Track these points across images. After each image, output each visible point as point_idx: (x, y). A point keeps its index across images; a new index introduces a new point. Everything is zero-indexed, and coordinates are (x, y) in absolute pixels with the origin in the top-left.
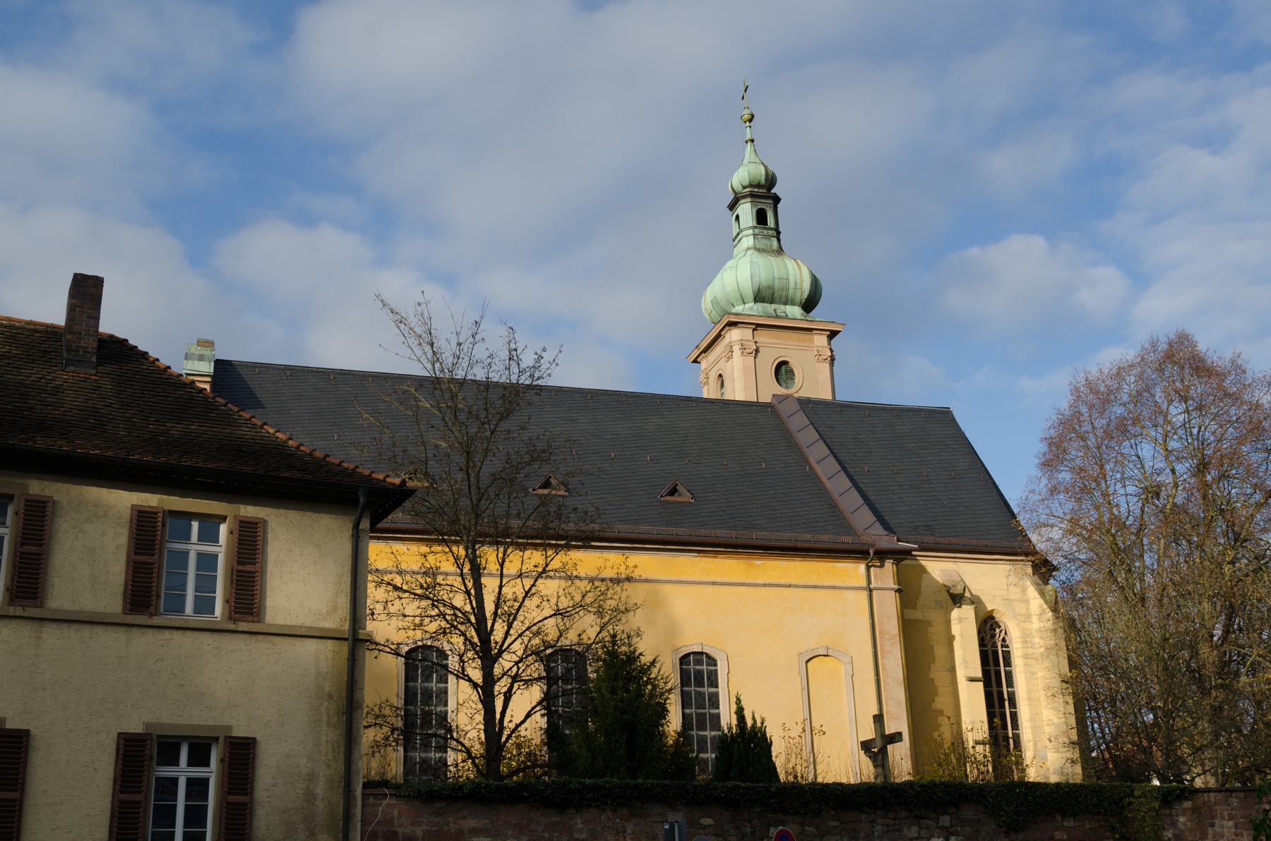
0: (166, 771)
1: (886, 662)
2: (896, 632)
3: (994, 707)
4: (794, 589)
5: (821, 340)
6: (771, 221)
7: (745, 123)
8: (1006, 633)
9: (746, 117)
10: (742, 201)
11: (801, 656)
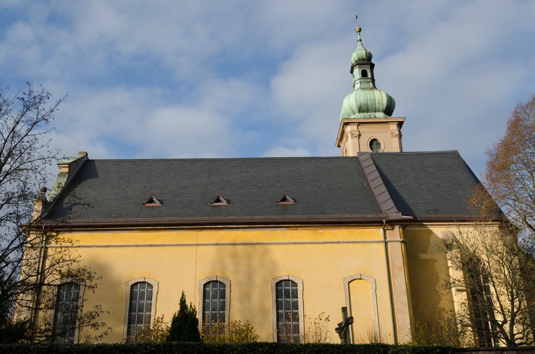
1: (396, 281)
2: (402, 264)
4: (342, 244)
5: (394, 127)
6: (369, 75)
7: (357, 33)
9: (357, 30)
10: (355, 68)
11: (345, 280)
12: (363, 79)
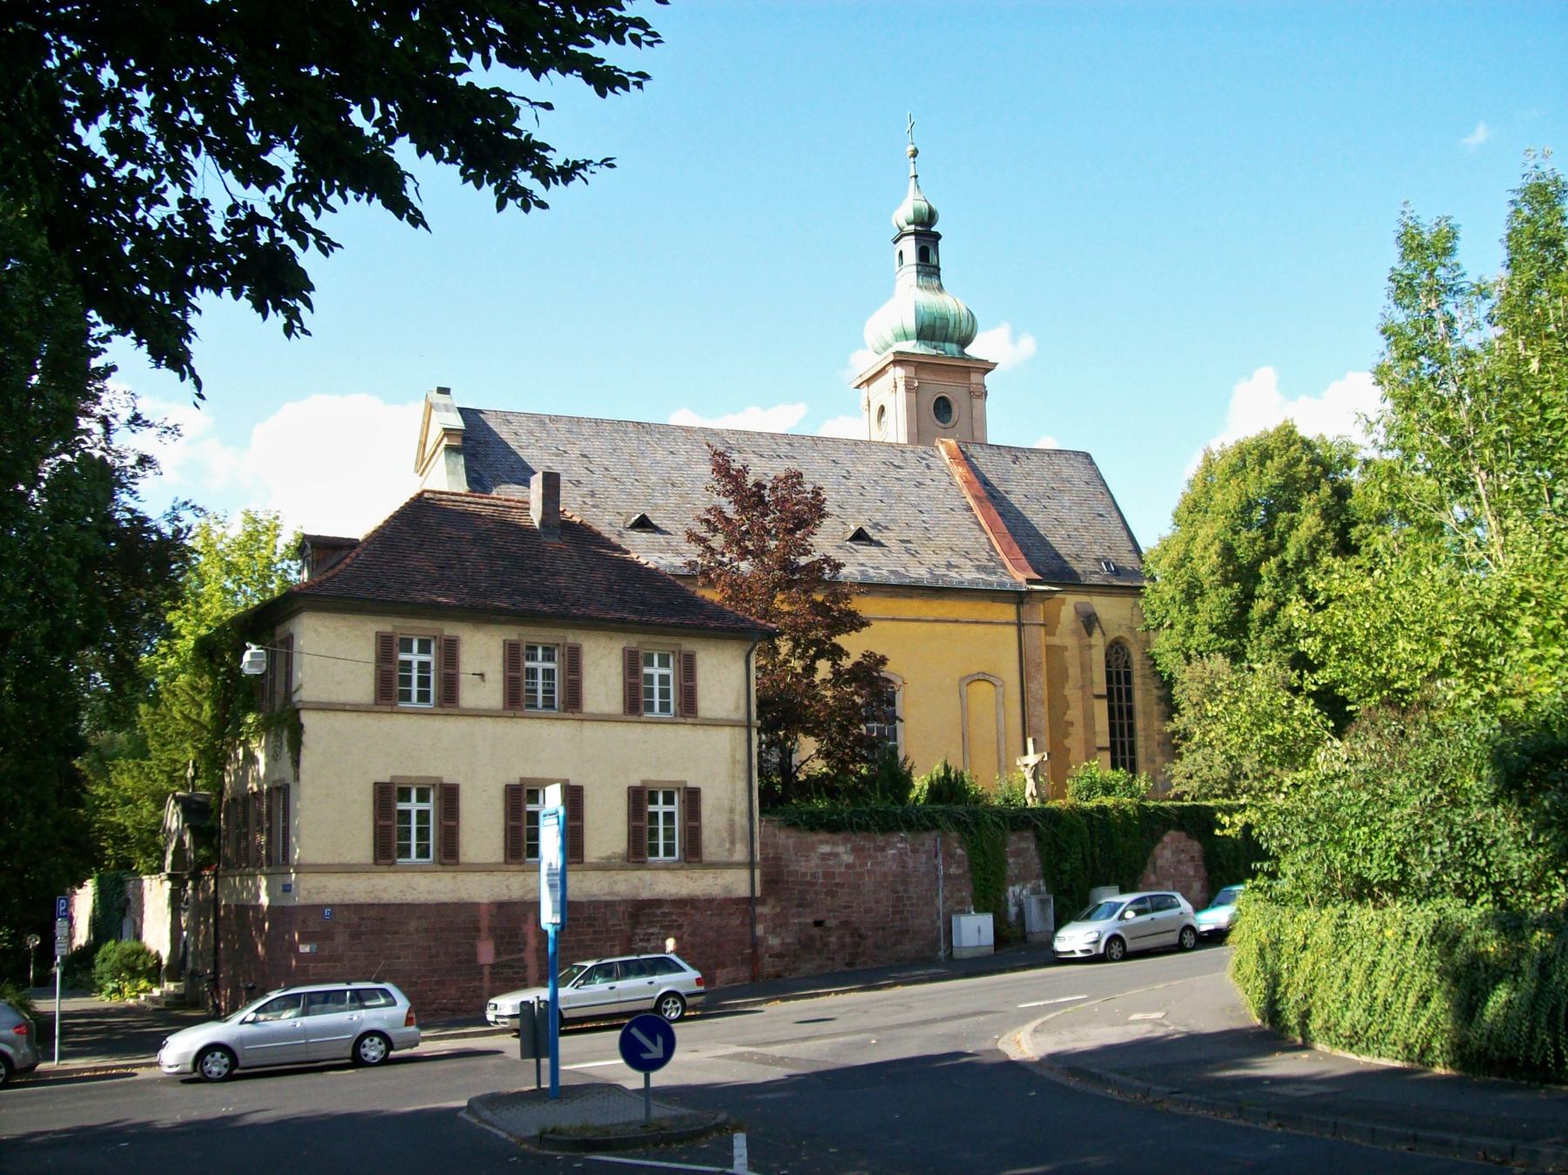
0: (651, 808)
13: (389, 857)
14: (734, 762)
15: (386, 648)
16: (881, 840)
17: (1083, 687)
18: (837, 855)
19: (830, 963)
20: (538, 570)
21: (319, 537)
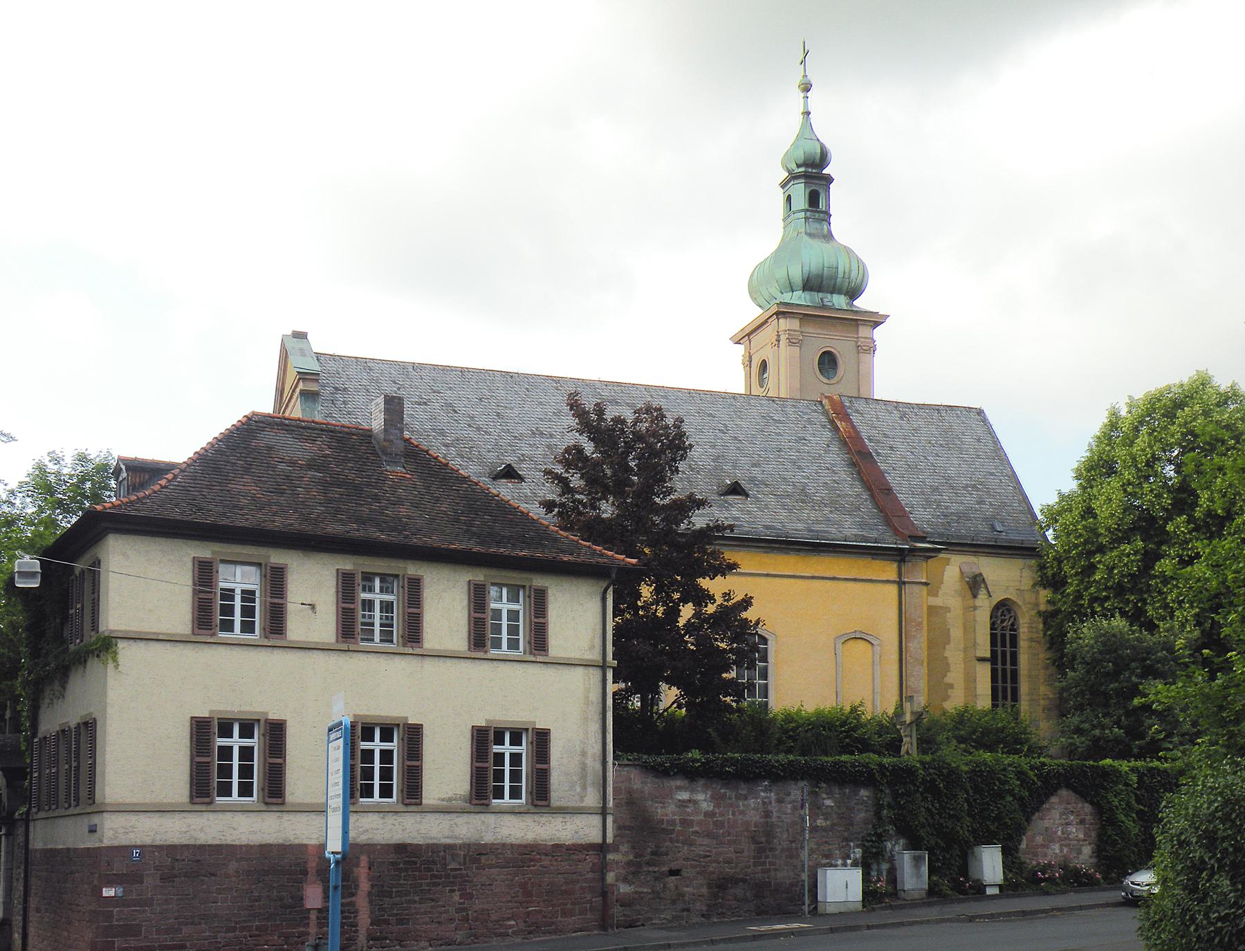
0: (497, 749)
3: (997, 682)
8: (1015, 619)
12: (812, 211)
13: (208, 795)
14: (587, 702)
15: (204, 574)
16: (743, 791)
17: (965, 650)
18: (695, 802)
19: (685, 913)
20: (376, 498)
21: (136, 459)
